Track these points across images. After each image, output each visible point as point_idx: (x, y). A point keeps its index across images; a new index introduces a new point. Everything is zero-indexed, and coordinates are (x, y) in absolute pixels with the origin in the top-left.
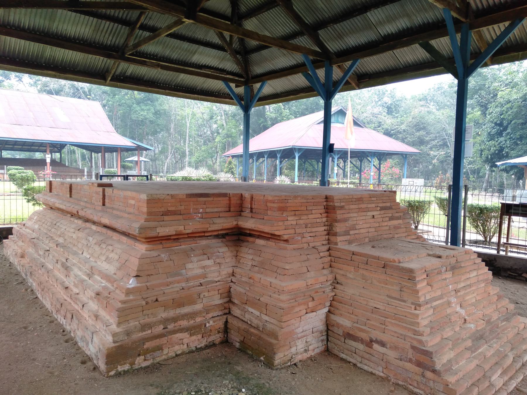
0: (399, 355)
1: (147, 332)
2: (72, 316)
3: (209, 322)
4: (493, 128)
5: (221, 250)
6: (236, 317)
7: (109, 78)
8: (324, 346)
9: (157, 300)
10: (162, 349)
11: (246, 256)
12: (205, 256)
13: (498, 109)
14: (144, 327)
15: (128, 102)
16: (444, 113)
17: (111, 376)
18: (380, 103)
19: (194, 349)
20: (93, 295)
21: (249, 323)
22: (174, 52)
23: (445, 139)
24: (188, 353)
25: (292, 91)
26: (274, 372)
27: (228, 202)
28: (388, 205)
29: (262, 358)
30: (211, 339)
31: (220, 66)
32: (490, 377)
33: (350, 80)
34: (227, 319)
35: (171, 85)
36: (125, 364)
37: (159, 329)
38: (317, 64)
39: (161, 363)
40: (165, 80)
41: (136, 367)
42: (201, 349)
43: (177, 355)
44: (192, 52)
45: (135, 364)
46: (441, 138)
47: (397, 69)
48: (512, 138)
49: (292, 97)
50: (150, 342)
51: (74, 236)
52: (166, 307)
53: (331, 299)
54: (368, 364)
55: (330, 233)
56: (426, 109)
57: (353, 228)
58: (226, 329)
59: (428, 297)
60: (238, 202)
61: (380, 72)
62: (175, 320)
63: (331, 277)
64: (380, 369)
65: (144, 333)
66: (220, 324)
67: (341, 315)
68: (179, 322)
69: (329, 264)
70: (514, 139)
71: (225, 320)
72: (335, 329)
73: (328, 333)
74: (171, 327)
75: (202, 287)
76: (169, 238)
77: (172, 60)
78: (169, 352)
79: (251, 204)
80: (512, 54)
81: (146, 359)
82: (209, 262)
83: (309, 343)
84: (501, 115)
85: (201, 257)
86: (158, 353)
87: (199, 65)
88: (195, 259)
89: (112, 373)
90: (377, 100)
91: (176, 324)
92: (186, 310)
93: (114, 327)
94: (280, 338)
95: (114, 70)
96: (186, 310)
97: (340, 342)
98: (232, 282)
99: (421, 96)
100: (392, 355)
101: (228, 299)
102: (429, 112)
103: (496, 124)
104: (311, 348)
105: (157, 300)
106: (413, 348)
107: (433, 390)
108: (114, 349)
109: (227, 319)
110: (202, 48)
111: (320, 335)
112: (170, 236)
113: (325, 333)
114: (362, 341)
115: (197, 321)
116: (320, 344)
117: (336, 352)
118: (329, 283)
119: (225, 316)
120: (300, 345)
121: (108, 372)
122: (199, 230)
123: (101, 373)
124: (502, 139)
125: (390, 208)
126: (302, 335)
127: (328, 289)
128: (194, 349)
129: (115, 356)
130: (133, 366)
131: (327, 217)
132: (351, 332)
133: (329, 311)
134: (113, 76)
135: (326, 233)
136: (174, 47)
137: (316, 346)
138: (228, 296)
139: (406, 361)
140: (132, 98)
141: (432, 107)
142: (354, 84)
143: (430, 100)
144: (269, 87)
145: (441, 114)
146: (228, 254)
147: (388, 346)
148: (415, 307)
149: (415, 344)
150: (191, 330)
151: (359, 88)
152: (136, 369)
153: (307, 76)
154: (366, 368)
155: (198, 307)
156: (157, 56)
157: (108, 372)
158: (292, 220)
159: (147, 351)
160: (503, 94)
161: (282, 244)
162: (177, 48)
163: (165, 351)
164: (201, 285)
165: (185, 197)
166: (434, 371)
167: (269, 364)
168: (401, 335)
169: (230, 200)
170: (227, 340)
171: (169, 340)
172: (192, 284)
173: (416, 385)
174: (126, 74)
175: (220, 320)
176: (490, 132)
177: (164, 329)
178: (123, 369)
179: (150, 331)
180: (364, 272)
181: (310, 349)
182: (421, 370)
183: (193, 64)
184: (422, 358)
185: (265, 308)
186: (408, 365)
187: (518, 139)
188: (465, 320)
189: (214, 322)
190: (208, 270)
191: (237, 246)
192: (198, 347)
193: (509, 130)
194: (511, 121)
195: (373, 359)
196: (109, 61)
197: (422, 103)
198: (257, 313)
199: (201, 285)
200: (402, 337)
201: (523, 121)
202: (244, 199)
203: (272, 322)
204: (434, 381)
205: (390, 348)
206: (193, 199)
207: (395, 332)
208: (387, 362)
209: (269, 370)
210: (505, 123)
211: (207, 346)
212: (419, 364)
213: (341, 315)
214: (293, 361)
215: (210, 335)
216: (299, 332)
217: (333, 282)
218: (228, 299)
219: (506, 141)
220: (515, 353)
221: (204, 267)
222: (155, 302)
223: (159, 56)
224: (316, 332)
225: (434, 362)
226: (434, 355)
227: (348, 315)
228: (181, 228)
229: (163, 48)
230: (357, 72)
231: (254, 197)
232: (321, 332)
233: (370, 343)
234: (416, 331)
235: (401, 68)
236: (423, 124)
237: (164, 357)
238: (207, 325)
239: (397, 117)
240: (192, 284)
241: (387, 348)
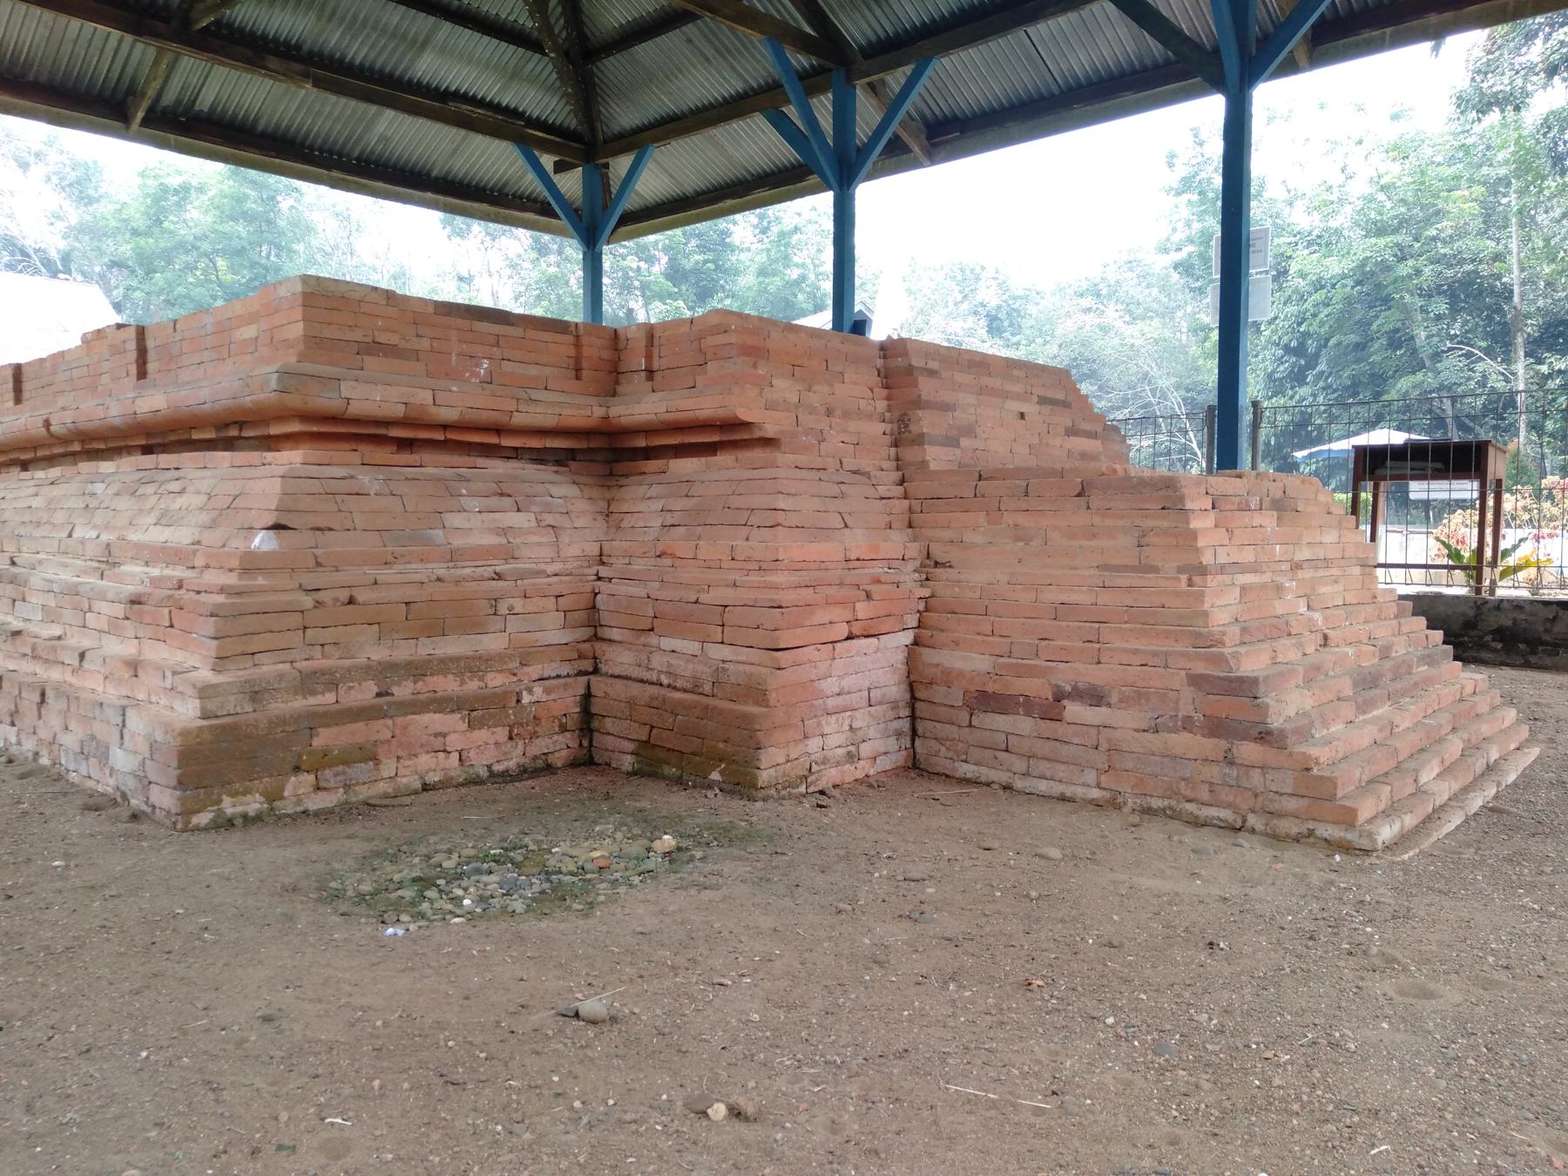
0: (1150, 715)
1: (319, 699)
2: (43, 695)
3: (530, 691)
4: (1280, 361)
5: (555, 490)
6: (619, 677)
7: (140, 115)
8: (904, 753)
9: (351, 601)
10: (375, 759)
11: (641, 506)
12: (507, 501)
13: (1292, 309)
14: (308, 682)
15: (198, 292)
16: (1146, 329)
17: (198, 829)
18: (965, 306)
19: (484, 773)
20: (119, 610)
21: (666, 682)
22: (354, 37)
23: (1149, 405)
24: (462, 785)
25: (728, 186)
26: (759, 805)
27: (572, 351)
28: (1060, 396)
29: (715, 776)
30: (539, 746)
31: (506, 99)
32: (1416, 771)
33: (905, 136)
34: (589, 687)
35: (348, 155)
36: (246, 792)
37: (365, 693)
38: (811, 82)
39: (372, 801)
40: (328, 135)
41: (286, 807)
42: (506, 777)
43: (426, 787)
44: (414, 41)
45: (282, 798)
46: (1140, 402)
47: (1042, 98)
48: (1330, 386)
49: (729, 202)
50: (334, 730)
51: (36, 502)
52: (383, 627)
53: (921, 607)
54: (1048, 774)
55: (902, 437)
56: (1097, 321)
57: (970, 431)
58: (587, 720)
59: (1223, 559)
60: (607, 354)
61: (993, 111)
62: (418, 670)
63: (914, 550)
64: (1090, 777)
65: (312, 701)
66: (567, 701)
67: (956, 643)
68: (428, 679)
69: (906, 517)
70: (1335, 391)
71: (582, 691)
72: (939, 693)
73: (913, 709)
74: (403, 691)
75: (500, 583)
76: (382, 431)
77: (351, 65)
78: (400, 772)
79: (649, 357)
80: (1366, 35)
81: (323, 784)
82: (522, 520)
83: (860, 734)
84: (1300, 324)
85: (494, 502)
86: (360, 771)
87: (437, 88)
88: (475, 504)
89: (203, 818)
90: (959, 298)
91: (420, 684)
92: (452, 646)
93: (206, 675)
94: (773, 698)
95: (156, 85)
96: (452, 646)
97: (955, 728)
98: (599, 579)
99: (1085, 285)
100: (1124, 721)
101: (590, 631)
102: (1105, 330)
103: (1287, 349)
104: (865, 750)
105: (351, 601)
106: (1195, 680)
107: (1260, 799)
108: (207, 736)
109: (589, 687)
110: (447, 27)
111: (891, 714)
112: (387, 423)
113: (907, 712)
114: (1027, 705)
115: (491, 684)
116: (892, 744)
117: (942, 764)
118: (911, 566)
119: (583, 679)
120: (832, 737)
121: (187, 813)
122: (485, 417)
123: (159, 824)
124: (1304, 391)
125: (1065, 404)
126: (840, 701)
127: (908, 576)
128: (484, 773)
129: (214, 762)
130: (277, 804)
131: (889, 398)
132: (990, 688)
133: (916, 643)
134: (150, 110)
135: (888, 439)
136: (355, 18)
137: (881, 748)
138: (591, 620)
139: (1175, 730)
140: (211, 282)
141: (1112, 314)
142: (916, 149)
143: (1109, 297)
144: (655, 177)
145: (1137, 334)
146: (582, 505)
147: (1114, 699)
148: (1190, 579)
149: (1200, 668)
150: (476, 710)
151: (933, 162)
152: (288, 815)
153: (781, 123)
154: (1043, 786)
155: (492, 643)
156: (298, 47)
157: (187, 813)
158: (785, 389)
159: (324, 760)
160: (1304, 262)
161: (758, 454)
162: (364, 25)
163: (388, 767)
164: (499, 577)
165: (431, 310)
166: (1264, 736)
167: (742, 784)
168: (1155, 654)
169: (578, 345)
170: (591, 757)
171: (397, 732)
172: (468, 571)
173: (1205, 795)
174: (197, 107)
175: (566, 686)
176: (1273, 372)
177: (379, 695)
178: (239, 809)
179: (330, 698)
180: (1022, 520)
181: (863, 755)
182: (1223, 744)
183: (419, 83)
184: (1224, 706)
185: (717, 621)
186: (1181, 741)
187: (1346, 388)
188: (1326, 637)
189: (547, 691)
190: (518, 541)
191: (609, 487)
192: (497, 768)
193: (1322, 367)
194: (1327, 340)
195: (1065, 751)
196: (139, 47)
197: (1087, 302)
198: (692, 647)
199: (499, 577)
200: (1156, 661)
201: (1358, 339)
202: (622, 345)
203: (740, 658)
204: (1263, 768)
205: (1121, 701)
206: (459, 321)
207: (1136, 652)
208: (1113, 749)
209: (737, 804)
210: (1312, 347)
211: (525, 771)
212: (1216, 727)
213: (956, 643)
214: (813, 783)
215: (534, 735)
216: (829, 693)
217: (922, 565)
218: (590, 631)
219: (1314, 396)
220: (1466, 736)
221: (504, 531)
222: (344, 604)
223: (306, 48)
224: (880, 703)
225: (1263, 710)
226: (1262, 689)
227: (980, 638)
228: (424, 397)
229: (319, 19)
230: (927, 112)
231: (657, 335)
232: (894, 706)
233: (1051, 709)
234: (1199, 635)
235: (1053, 95)
236: (1087, 361)
237: (382, 787)
238: (526, 699)
239: (1018, 344)
240: (468, 571)
241: (1109, 705)
